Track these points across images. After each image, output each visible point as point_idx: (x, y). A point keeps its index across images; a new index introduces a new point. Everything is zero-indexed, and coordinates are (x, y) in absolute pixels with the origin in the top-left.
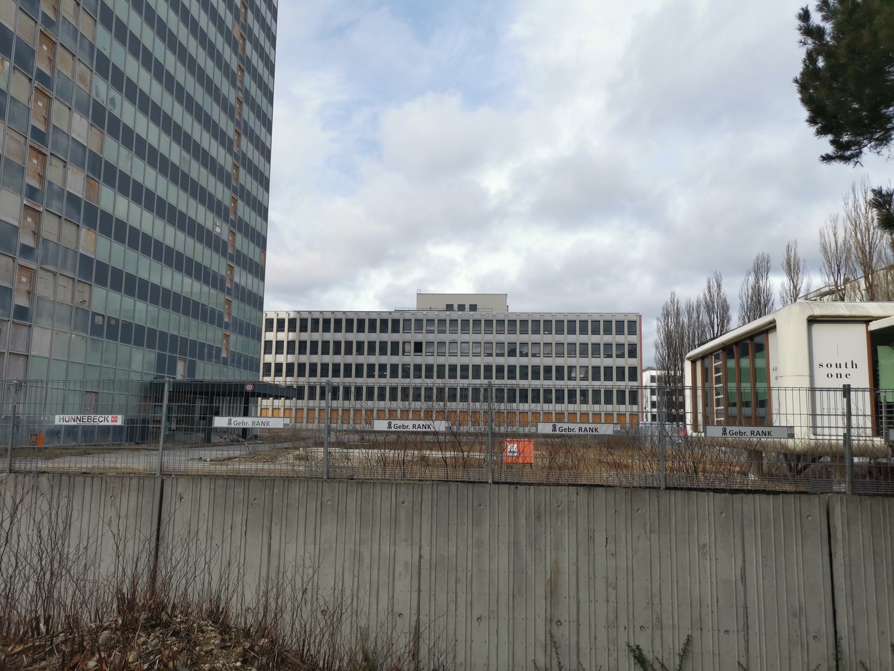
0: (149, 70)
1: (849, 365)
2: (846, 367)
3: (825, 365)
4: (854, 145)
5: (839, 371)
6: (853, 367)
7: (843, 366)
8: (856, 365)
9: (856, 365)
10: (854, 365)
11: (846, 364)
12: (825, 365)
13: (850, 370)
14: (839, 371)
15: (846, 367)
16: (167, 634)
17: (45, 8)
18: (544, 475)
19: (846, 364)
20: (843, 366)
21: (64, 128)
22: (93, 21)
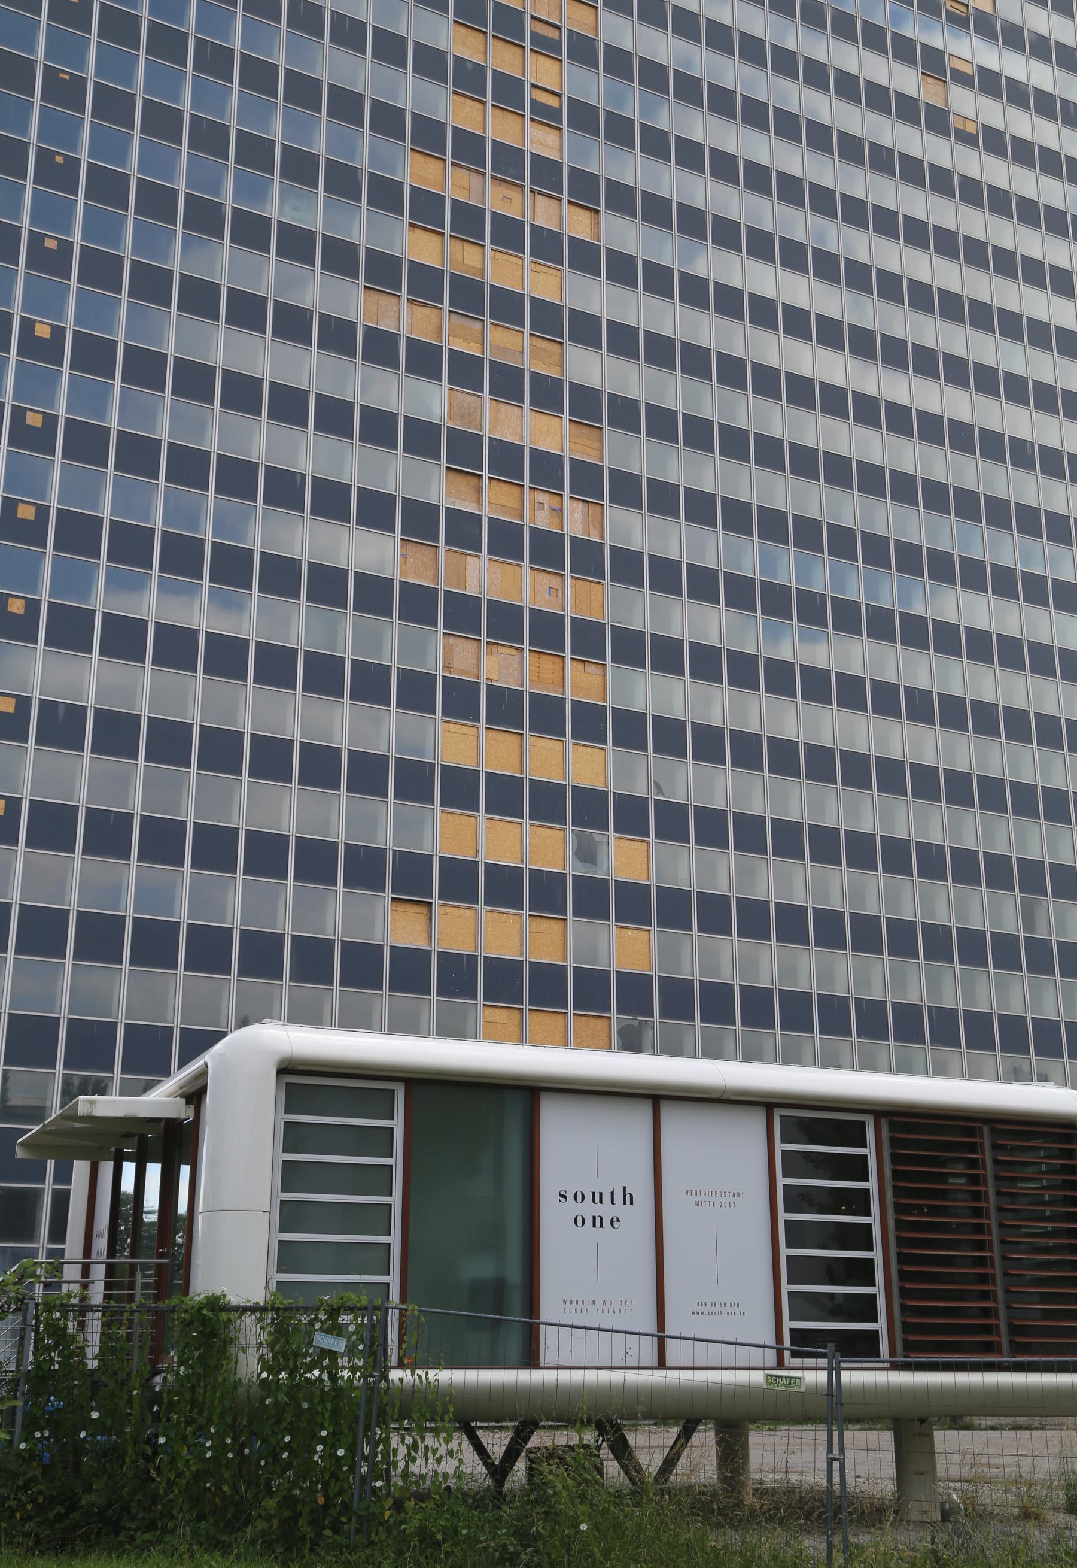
0: (157, 1084)
1: (618, 1197)
2: (612, 1202)
3: (570, 1197)
4: (898, 1496)
5: (598, 1210)
6: (625, 1203)
7: (606, 1198)
8: (631, 1196)
9: (631, 1196)
10: (628, 1199)
11: (612, 1193)
12: (570, 1197)
13: (618, 1209)
14: (598, 1210)
15: (612, 1202)
16: (597, 1482)
17: (988, 1567)
18: (954, 1471)
19: (612, 1193)
20: (606, 1198)
21: (134, 1454)
22: (941, 83)
